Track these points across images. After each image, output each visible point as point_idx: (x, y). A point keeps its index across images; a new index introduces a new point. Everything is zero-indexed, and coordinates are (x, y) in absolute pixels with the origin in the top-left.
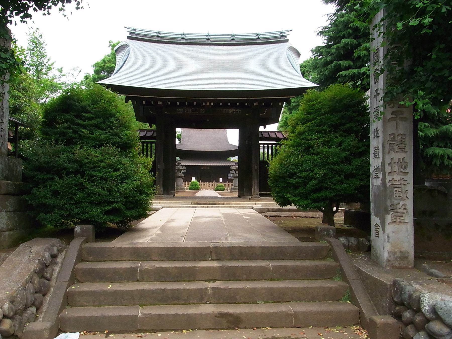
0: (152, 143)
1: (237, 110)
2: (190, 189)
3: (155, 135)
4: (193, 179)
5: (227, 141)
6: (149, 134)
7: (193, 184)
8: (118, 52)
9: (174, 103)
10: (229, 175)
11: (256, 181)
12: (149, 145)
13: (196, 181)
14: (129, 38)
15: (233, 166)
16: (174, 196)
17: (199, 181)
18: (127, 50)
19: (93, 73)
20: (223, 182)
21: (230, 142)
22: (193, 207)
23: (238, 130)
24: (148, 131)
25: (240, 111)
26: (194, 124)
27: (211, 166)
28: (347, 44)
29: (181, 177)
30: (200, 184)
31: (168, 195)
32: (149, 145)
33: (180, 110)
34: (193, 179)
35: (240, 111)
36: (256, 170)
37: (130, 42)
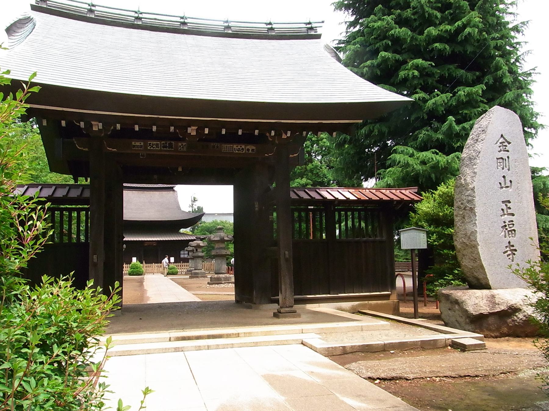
0: (79, 210)
1: (248, 147)
2: (130, 274)
3: (87, 194)
4: (134, 259)
6: (74, 193)
7: (134, 267)
8: (11, 31)
9: (127, 132)
10: (182, 252)
11: (288, 281)
12: (75, 214)
13: (138, 263)
17: (142, 263)
18: (30, 25)
20: (175, 262)
22: (177, 350)
23: (232, 186)
24: (71, 186)
25: (254, 148)
26: (156, 177)
28: (385, 60)
30: (143, 267)
32: (75, 214)
33: (138, 144)
34: (134, 259)
35: (254, 148)
36: (287, 260)
37: (38, 16)
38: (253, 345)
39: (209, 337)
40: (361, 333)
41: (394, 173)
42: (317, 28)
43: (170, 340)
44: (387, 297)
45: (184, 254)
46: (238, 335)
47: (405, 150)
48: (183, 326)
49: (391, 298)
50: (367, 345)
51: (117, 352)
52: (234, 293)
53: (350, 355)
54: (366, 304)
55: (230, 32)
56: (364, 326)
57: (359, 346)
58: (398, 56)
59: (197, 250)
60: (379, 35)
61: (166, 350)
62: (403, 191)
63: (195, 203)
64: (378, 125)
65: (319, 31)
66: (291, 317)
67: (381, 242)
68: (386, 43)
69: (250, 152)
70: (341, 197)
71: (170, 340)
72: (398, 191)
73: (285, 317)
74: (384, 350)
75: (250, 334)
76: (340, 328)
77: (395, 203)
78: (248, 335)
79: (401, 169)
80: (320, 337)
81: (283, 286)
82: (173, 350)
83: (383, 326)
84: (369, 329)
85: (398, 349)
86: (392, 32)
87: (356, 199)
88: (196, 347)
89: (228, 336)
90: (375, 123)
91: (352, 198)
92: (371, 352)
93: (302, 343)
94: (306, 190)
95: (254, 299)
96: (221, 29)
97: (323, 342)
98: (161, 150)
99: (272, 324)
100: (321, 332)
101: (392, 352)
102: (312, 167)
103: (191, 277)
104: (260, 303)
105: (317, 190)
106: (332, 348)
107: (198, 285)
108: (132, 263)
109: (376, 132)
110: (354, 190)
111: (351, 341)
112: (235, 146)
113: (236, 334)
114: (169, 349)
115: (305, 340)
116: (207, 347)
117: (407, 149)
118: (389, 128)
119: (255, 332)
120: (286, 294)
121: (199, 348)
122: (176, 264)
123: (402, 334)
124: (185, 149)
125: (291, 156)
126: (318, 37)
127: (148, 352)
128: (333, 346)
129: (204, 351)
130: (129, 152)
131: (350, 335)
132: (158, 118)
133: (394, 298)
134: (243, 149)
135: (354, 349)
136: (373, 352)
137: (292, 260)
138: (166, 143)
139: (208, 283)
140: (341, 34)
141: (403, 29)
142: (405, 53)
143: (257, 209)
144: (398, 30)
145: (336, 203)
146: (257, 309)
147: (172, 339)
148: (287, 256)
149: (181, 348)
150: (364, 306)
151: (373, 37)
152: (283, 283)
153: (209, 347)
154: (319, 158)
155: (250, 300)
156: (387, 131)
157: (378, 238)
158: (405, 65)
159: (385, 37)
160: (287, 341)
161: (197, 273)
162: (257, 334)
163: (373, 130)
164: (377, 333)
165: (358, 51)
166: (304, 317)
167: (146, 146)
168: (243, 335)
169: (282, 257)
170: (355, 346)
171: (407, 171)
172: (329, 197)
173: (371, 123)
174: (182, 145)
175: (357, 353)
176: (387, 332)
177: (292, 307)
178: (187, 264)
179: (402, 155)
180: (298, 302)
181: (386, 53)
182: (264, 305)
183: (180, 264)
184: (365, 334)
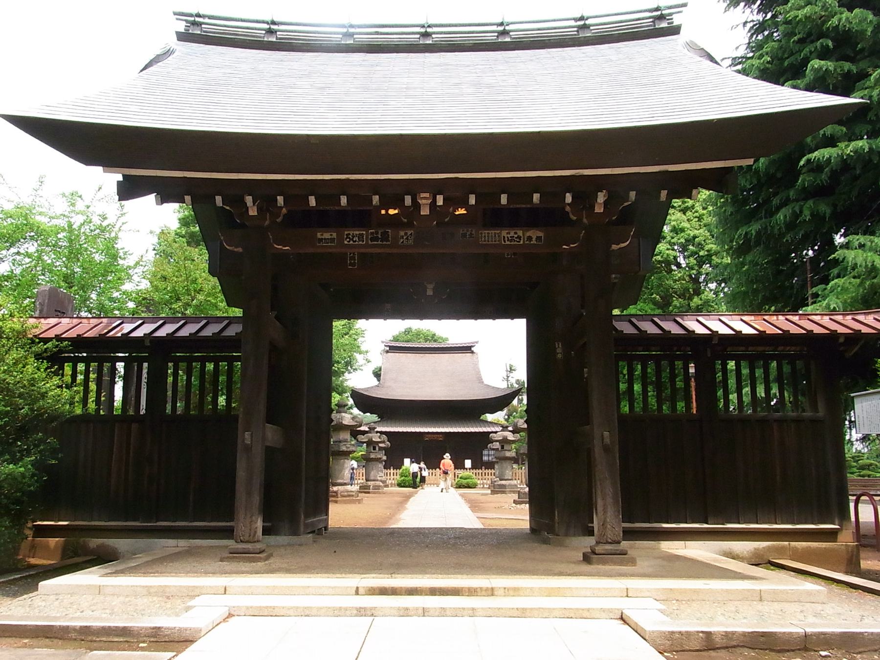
1: (528, 234)
2: (399, 485)
5: (480, 380)
10: (485, 452)
11: (609, 490)
14: (183, 37)
15: (496, 432)
16: (321, 531)
19: (177, 225)
20: (474, 467)
21: (486, 381)
22: (361, 612)
25: (541, 234)
27: (398, 432)
29: (378, 460)
31: (295, 532)
33: (327, 236)
35: (541, 234)
36: (606, 449)
38: (516, 613)
39: (433, 592)
40: (759, 606)
41: (844, 290)
42: (674, 16)
43: (357, 593)
44: (831, 535)
45: (487, 456)
46: (491, 592)
47: (869, 244)
48: (397, 568)
49: (840, 537)
50: (764, 634)
51: (247, 608)
52: (528, 518)
53: (722, 653)
54: (783, 547)
55: (508, 39)
56: (766, 591)
57: (744, 634)
58: (847, 66)
59: (502, 447)
60: (809, 34)
61: (339, 612)
62: (861, 318)
63: (511, 375)
64: (810, 203)
65: (677, 20)
66: (615, 563)
67: (813, 421)
68: (822, 44)
69: (534, 242)
70: (723, 330)
71: (357, 593)
72: (849, 317)
73: (604, 563)
74: (806, 649)
75: (516, 591)
76: (711, 591)
77: (842, 340)
78: (511, 592)
79: (858, 281)
80: (662, 607)
81: (600, 503)
82: (355, 612)
83: (809, 593)
84: (777, 597)
85: (839, 649)
86: (834, 21)
87: (756, 332)
88: (399, 609)
89: (472, 592)
90: (806, 199)
91: (747, 330)
92: (772, 650)
93: (622, 618)
94: (656, 319)
95: (557, 525)
96: (491, 37)
97: (668, 619)
98: (367, 246)
99: (569, 575)
100: (666, 598)
101: (823, 653)
102: (700, 302)
103: (494, 492)
104: (574, 535)
105: (678, 319)
106: (680, 632)
107: (497, 505)
108: (403, 468)
109: (807, 215)
110: (753, 318)
111: (731, 620)
112: (504, 233)
113: (487, 589)
114: (346, 609)
115: (627, 613)
116: (421, 611)
117: (872, 242)
118: (835, 206)
119: (526, 588)
120: (607, 515)
121: (405, 612)
122: (474, 471)
123: (856, 613)
124: (411, 242)
125: (614, 247)
126: (675, 30)
127: (306, 613)
128: (684, 629)
129: (415, 618)
130: (311, 250)
131: (733, 609)
132: (348, 180)
133: (846, 539)
134: (519, 237)
135: (731, 639)
136: (779, 651)
137: (617, 448)
138: (377, 233)
139: (515, 502)
140: (737, 48)
141: (857, 11)
142: (865, 58)
143: (559, 356)
144: (846, 14)
145: (715, 341)
146: (561, 545)
147: (361, 591)
148: (607, 440)
149: (371, 609)
150: (781, 552)
151: (796, 38)
152: (599, 492)
153: (425, 612)
154: (713, 286)
155: (551, 530)
156: (828, 212)
157: (808, 414)
158: (863, 82)
159: (822, 35)
160: (588, 610)
161: (504, 486)
162: (531, 592)
163: (801, 212)
164: (795, 607)
165: (768, 69)
166: (643, 564)
167: (340, 238)
168: (501, 592)
169: (597, 442)
170: (733, 633)
171: (872, 286)
172: (700, 330)
173: (797, 200)
174: (406, 234)
175: (739, 650)
176: (819, 607)
177: (619, 543)
178: (493, 471)
179: (860, 251)
180: (629, 535)
181: (823, 62)
182: (573, 538)
183: (480, 471)
184: (765, 607)
